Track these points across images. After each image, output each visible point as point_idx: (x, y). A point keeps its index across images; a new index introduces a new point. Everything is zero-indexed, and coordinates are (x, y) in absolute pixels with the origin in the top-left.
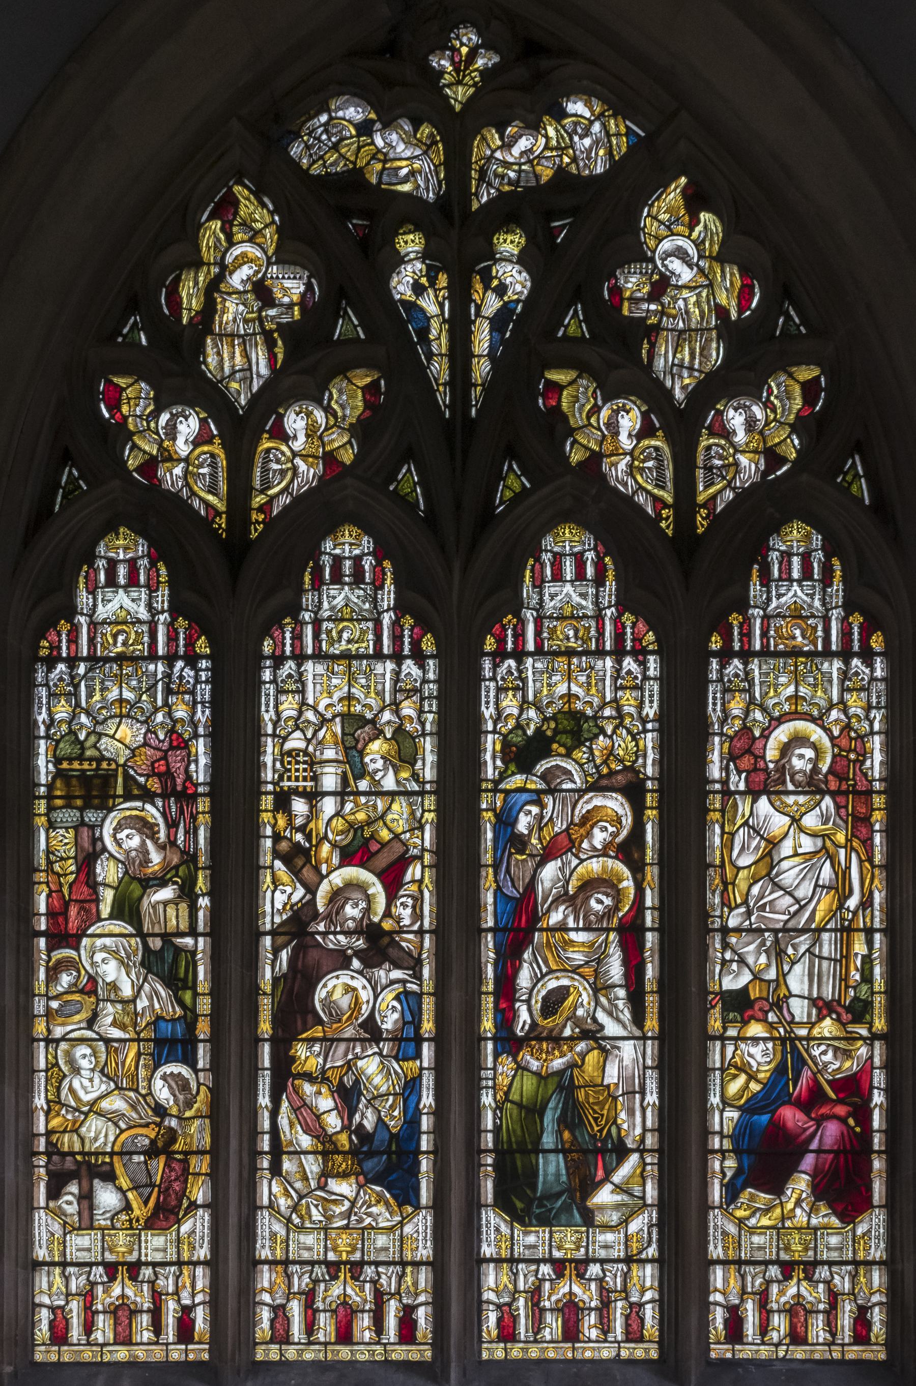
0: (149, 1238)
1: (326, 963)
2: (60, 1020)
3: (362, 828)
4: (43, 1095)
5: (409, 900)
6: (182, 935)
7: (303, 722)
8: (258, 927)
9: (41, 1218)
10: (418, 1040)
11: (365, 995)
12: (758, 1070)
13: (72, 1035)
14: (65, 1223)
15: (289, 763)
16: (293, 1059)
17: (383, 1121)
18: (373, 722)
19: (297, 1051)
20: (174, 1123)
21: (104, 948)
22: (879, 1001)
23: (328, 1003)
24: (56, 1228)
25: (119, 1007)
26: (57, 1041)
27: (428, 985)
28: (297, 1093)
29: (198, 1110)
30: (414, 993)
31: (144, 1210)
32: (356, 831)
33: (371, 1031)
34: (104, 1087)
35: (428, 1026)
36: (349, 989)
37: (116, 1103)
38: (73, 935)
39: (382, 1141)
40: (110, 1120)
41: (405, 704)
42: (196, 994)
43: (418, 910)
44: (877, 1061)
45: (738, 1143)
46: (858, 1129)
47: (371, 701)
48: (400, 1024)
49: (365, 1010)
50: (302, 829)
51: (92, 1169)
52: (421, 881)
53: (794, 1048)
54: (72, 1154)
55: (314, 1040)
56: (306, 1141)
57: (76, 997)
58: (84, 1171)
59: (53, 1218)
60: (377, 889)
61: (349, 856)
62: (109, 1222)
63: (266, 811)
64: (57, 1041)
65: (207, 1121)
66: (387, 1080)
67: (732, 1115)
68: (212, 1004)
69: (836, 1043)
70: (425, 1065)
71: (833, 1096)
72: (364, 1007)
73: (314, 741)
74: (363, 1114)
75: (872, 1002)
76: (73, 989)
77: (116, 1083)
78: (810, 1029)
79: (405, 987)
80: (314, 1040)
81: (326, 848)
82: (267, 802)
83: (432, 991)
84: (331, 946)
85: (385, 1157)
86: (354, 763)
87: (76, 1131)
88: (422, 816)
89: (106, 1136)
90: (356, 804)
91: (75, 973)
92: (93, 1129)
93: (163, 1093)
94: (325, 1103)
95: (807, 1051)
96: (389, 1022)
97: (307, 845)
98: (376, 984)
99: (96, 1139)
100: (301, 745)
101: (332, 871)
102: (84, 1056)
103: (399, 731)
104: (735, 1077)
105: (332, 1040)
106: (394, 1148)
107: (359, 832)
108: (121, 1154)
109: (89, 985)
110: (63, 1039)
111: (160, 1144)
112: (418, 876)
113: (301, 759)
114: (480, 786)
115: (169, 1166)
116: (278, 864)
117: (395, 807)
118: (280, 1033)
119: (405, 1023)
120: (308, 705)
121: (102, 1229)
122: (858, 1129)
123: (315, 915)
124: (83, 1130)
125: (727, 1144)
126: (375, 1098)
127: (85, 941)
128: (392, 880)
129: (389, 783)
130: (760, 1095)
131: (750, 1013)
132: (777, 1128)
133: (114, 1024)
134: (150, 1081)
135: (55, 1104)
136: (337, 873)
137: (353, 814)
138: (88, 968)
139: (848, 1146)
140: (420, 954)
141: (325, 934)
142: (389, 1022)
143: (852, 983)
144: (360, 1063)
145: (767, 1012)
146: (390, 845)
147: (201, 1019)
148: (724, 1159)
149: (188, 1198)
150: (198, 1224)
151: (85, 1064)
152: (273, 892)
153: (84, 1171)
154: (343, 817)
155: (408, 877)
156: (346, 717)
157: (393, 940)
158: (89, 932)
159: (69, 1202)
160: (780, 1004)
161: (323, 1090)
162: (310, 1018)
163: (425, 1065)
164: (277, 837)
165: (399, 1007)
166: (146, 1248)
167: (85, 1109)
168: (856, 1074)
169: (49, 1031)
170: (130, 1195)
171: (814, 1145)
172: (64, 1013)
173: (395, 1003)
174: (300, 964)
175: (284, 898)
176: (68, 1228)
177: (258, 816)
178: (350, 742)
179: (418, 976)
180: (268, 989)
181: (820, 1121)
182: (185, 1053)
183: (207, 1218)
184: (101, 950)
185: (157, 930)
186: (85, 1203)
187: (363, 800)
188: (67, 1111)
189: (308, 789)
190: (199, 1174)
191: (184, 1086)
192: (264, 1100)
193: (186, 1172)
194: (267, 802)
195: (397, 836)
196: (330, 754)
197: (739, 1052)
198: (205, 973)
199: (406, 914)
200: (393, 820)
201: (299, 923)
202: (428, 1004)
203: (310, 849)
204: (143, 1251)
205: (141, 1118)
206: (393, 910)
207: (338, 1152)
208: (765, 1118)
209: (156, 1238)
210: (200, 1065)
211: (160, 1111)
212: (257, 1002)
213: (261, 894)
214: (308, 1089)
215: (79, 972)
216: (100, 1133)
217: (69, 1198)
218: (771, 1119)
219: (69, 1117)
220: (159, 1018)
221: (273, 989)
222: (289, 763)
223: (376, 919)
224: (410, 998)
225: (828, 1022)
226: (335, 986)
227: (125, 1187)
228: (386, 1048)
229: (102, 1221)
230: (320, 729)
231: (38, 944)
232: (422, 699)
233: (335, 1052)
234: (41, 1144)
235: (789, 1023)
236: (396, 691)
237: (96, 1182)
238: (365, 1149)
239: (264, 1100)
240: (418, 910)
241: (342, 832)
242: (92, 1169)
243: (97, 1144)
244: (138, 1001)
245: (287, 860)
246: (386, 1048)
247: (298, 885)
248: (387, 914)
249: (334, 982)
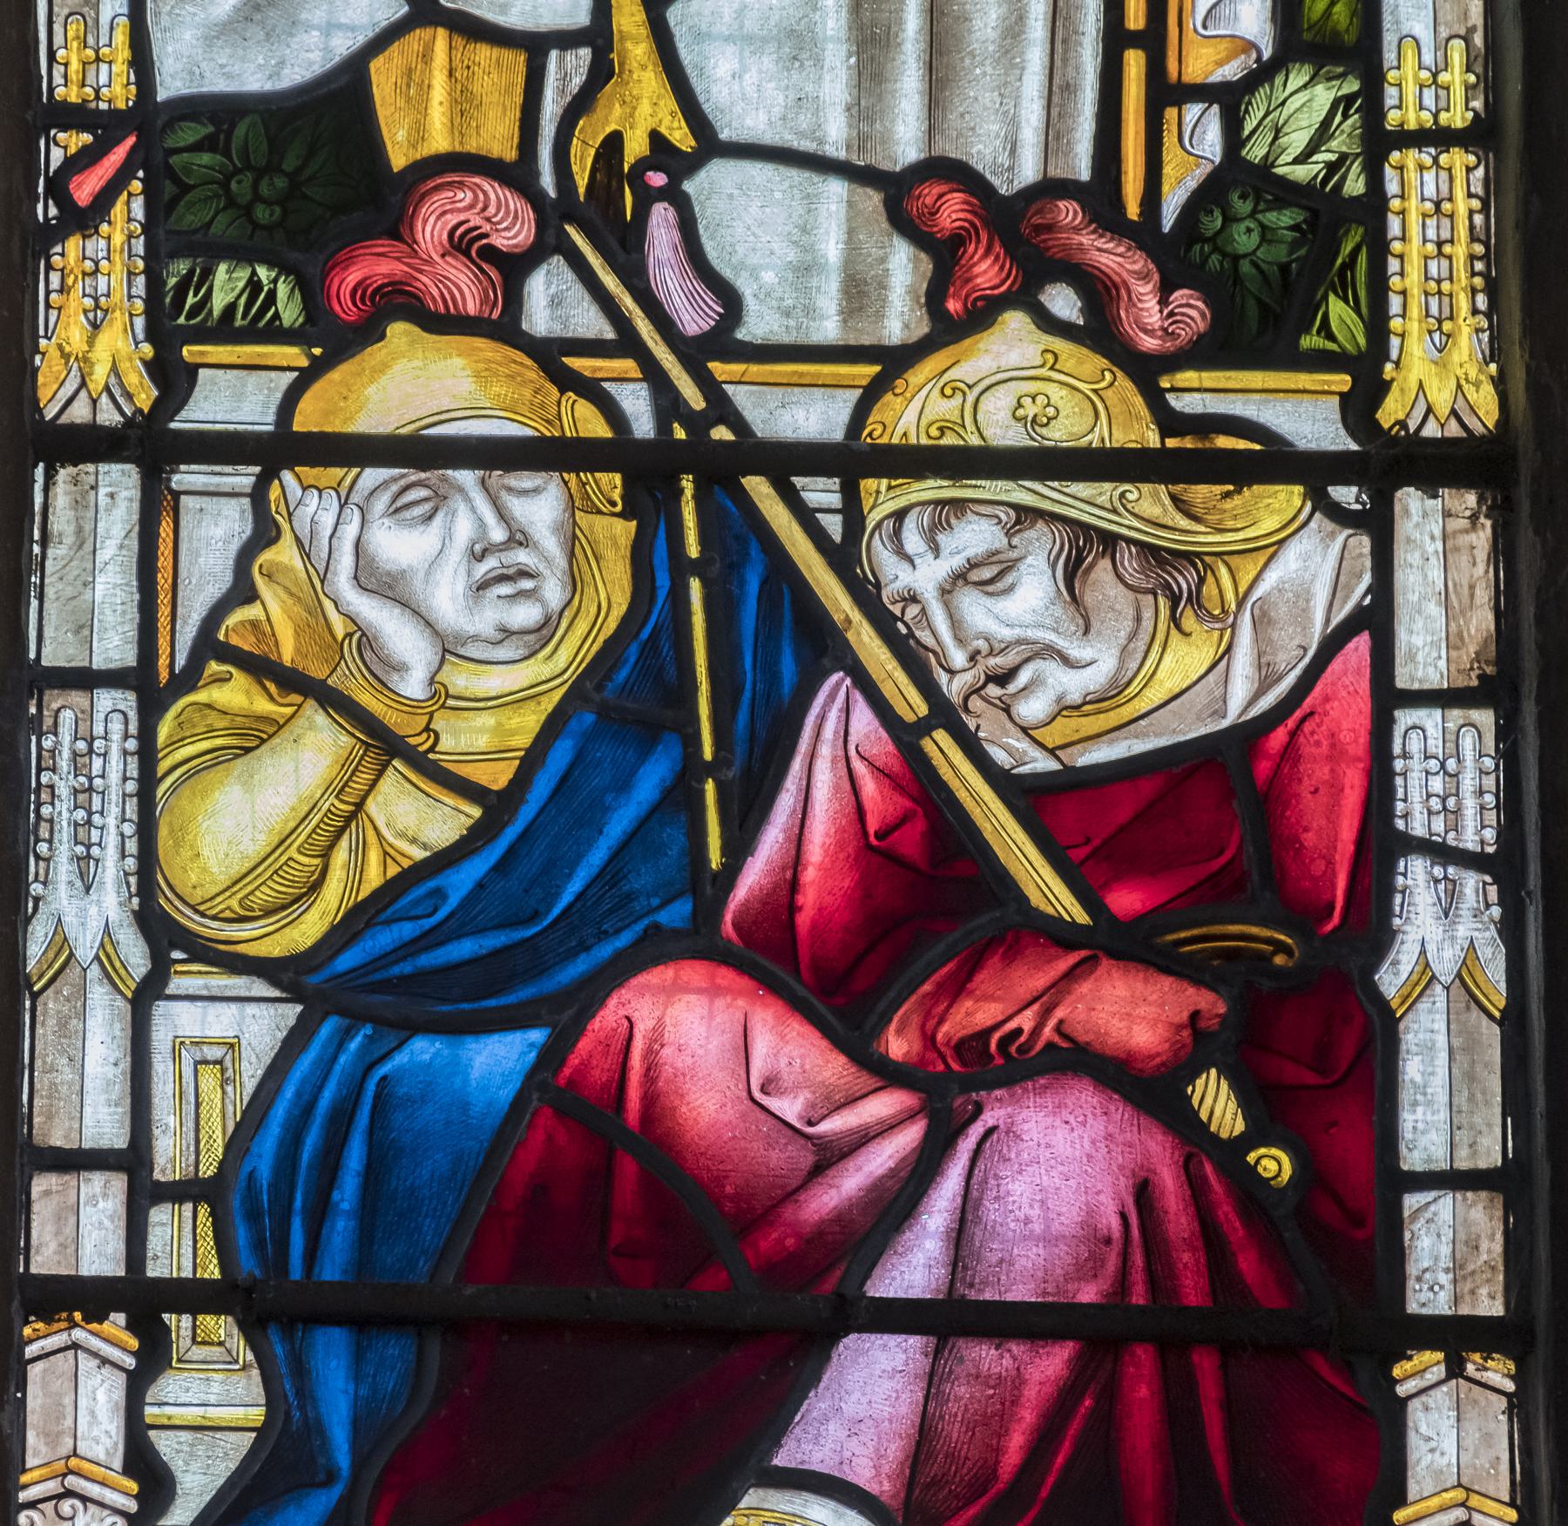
4: (113, 868)
12: (440, 695)
22: (1436, 214)
44: (1427, 648)
45: (273, 1250)
46: (1274, 1163)
53: (736, 531)
67: (231, 1029)
69: (1087, 500)
71: (1046, 888)
75: (1375, 205)
78: (871, 395)
95: (844, 558)
104: (252, 737)
122: (1274, 1163)
125: (180, 1245)
130: (461, 881)
131: (373, 266)
132: (591, 1147)
139: (1193, 1289)
143: (1201, 62)
145: (511, 270)
148: (153, 1358)
160: (611, 208)
168: (1250, 734)
171: (913, 1268)
181: (953, 1092)
197: (284, 553)
208: (497, 1061)
218: (550, 1057)
225: (1012, 342)
235: (695, 353)
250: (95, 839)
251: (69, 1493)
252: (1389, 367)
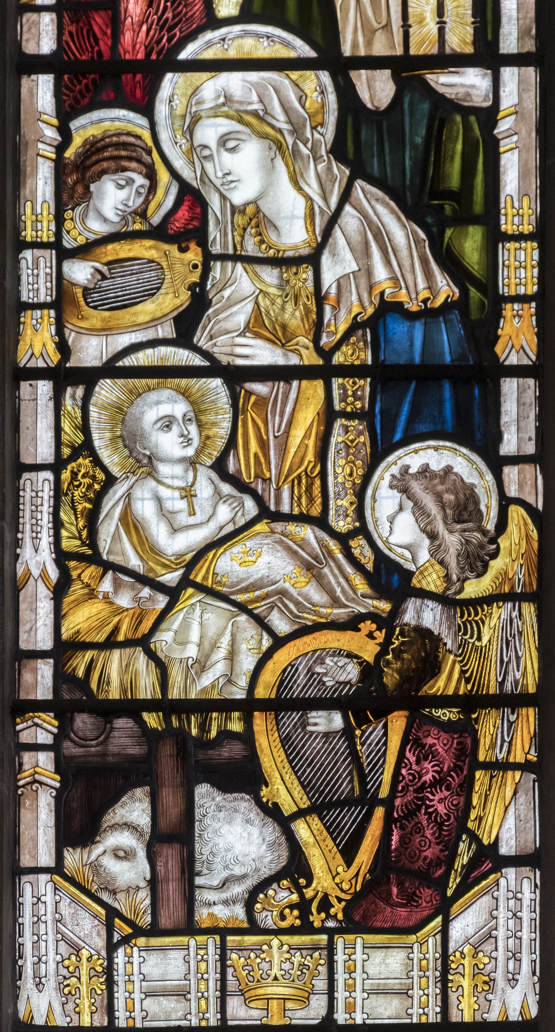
0: (359, 956)
2: (96, 318)
4: (46, 539)
6: (458, 61)
9: (39, 898)
13: (128, 361)
14: (112, 913)
20: (430, 616)
21: (227, 106)
24: (88, 928)
25: (270, 275)
26: (89, 378)
29: (504, 575)
31: (346, 875)
34: (224, 513)
37: (261, 561)
38: (134, 66)
40: (242, 608)
42: (495, 238)
51: (186, 752)
54: (132, 707)
57: (145, 249)
58: (167, 765)
59: (74, 900)
62: (240, 911)
64: (89, 378)
65: (529, 610)
68: (542, 264)
76: (135, 227)
77: (259, 500)
87: (144, 642)
89: (232, 656)
91: (140, 180)
92: (195, 635)
93: (399, 530)
99: (201, 665)
102: (167, 423)
108: (278, 706)
109: (183, 213)
110: (111, 369)
111: (390, 678)
114: (183, 713)
115: (418, 744)
121: (223, 932)
124: (164, 639)
127: (171, 84)
133: (257, 326)
134: (360, 494)
135: (79, 559)
138: (179, 164)
147: (509, 310)
149: (474, 838)
150: (502, 914)
151: (169, 444)
153: (167, 765)
158: (183, 55)
159: (121, 852)
166: (350, 988)
167: (171, 578)
169: (63, 347)
170: (302, 830)
172: (111, 300)
176: (122, 933)
182: (462, 411)
183: (528, 894)
184: (215, 113)
185: (380, 48)
186: (170, 858)
188: (117, 585)
190: (505, 766)
191: (464, 509)
193: (467, 757)
198: (523, 176)
204: (341, 995)
205: (336, 602)
209: (378, 956)
210: (509, 446)
211: (390, 579)
215: (151, 175)
216: (214, 646)
217: (124, 839)
219: (124, 600)
220: (388, 309)
227: (288, 808)
229: (218, 907)
231: (33, 94)
234: (40, 680)
237: (204, 793)
242: (186, 752)
243: (207, 680)
244: (326, 259)
250: (39, 517)
251: (35, 781)
252: (500, 330)
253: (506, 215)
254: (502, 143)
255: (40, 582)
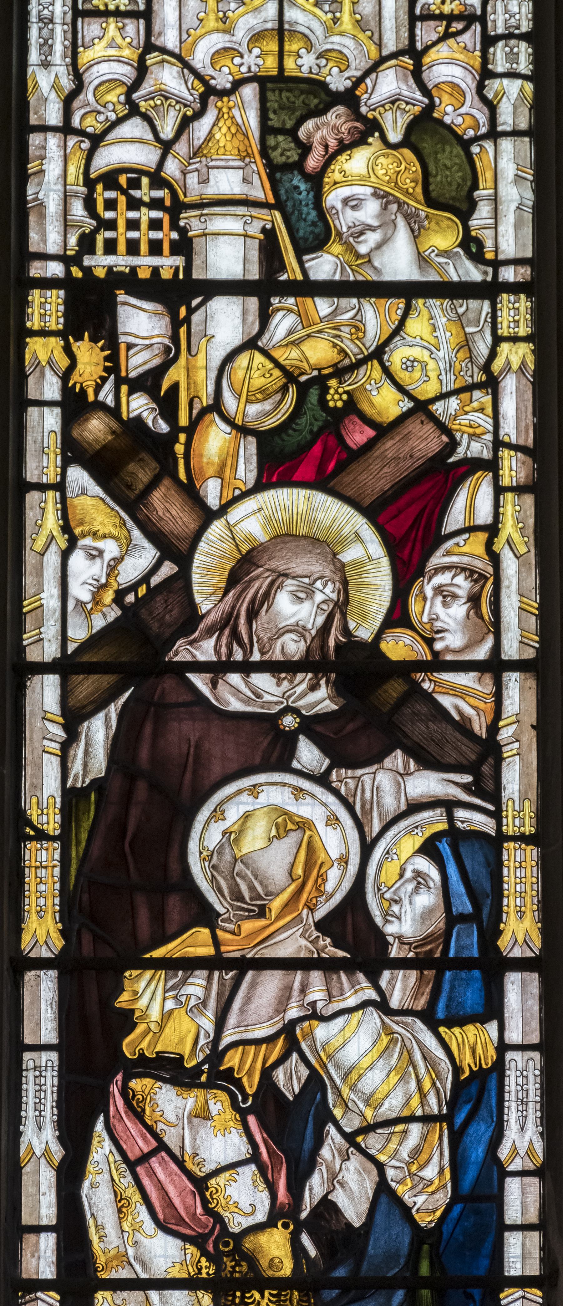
1: (222, 749)
3: (320, 381)
5: (460, 579)
7: (150, 97)
8: (21, 650)
10: (493, 967)
11: (337, 841)
15: (111, 205)
16: (127, 1021)
17: (392, 1193)
18: (349, 99)
19: (136, 997)
23: (230, 861)
27: (520, 814)
28: (139, 1115)
30: (478, 835)
32: (303, 390)
33: (354, 939)
35: (520, 931)
36: (287, 824)
39: (391, 1257)
41: (442, 51)
43: (485, 609)
47: (347, 45)
48: (438, 922)
49: (338, 884)
50: (149, 382)
52: (493, 530)
55: (190, 965)
56: (165, 1254)
60: (367, 549)
61: (282, 460)
63: (44, 333)
66: (403, 1078)
70: (514, 1036)
72: (333, 874)
73: (181, 148)
74: (333, 1176)
79: (451, 819)
80: (190, 965)
81: (215, 439)
82: (46, 309)
83: (528, 829)
84: (236, 705)
85: (399, 1296)
86: (297, 206)
88: (493, 354)
90: (304, 318)
94: (221, 1142)
96: (410, 913)
97: (163, 427)
98: (368, 809)
100: (145, 157)
101: (235, 500)
103: (425, 130)
105: (243, 965)
106: (425, 1269)
107: (314, 395)
112: (484, 515)
113: (144, 192)
116: (78, 476)
117: (416, 326)
118: (87, 948)
119: (452, 919)
120: (163, 50)
123: (190, 620)
126: (367, 1129)
128: (412, 525)
129: (398, 262)
136: (250, 504)
137: (296, 343)
140: (493, 729)
141: (217, 669)
142: (410, 913)
144: (322, 1031)
146: (404, 430)
152: (66, 555)
154: (265, 353)
155: (456, 517)
156: (273, 85)
157: (416, 687)
161: (214, 1108)
162: (174, 904)
163: (514, 1036)
164: (74, 405)
165: (434, 873)
173: (424, 864)
174: (144, 753)
175: (97, 569)
177: (21, 347)
178: (283, 149)
179: (488, 790)
180: (52, 823)
187: (323, 306)
189: (166, 274)
192: (40, 1137)
194: (46, 309)
195: (421, 408)
196: (227, 182)
199: (450, 621)
200: (410, 364)
201: (138, 650)
202: (521, 872)
203: (172, 438)
206: (414, 606)
207: (262, 1283)
212: (18, 858)
213: (30, 559)
214: (169, 1103)
221: (66, 824)
222: (111, 205)
223: (365, 633)
224: (464, 851)
226: (247, 816)
228: (401, 987)
230: (199, 114)
232: (488, 41)
233: (248, 1000)
236: (413, 19)
238: (341, 1272)
239: (40, 1137)
240: (485, 609)
241: (265, 394)
245: (105, 466)
246: (401, 987)
247: (137, 534)
248: (397, 616)
249: (245, 803)
253: (507, 817)
254: (504, 749)
255: (43, 1160)
